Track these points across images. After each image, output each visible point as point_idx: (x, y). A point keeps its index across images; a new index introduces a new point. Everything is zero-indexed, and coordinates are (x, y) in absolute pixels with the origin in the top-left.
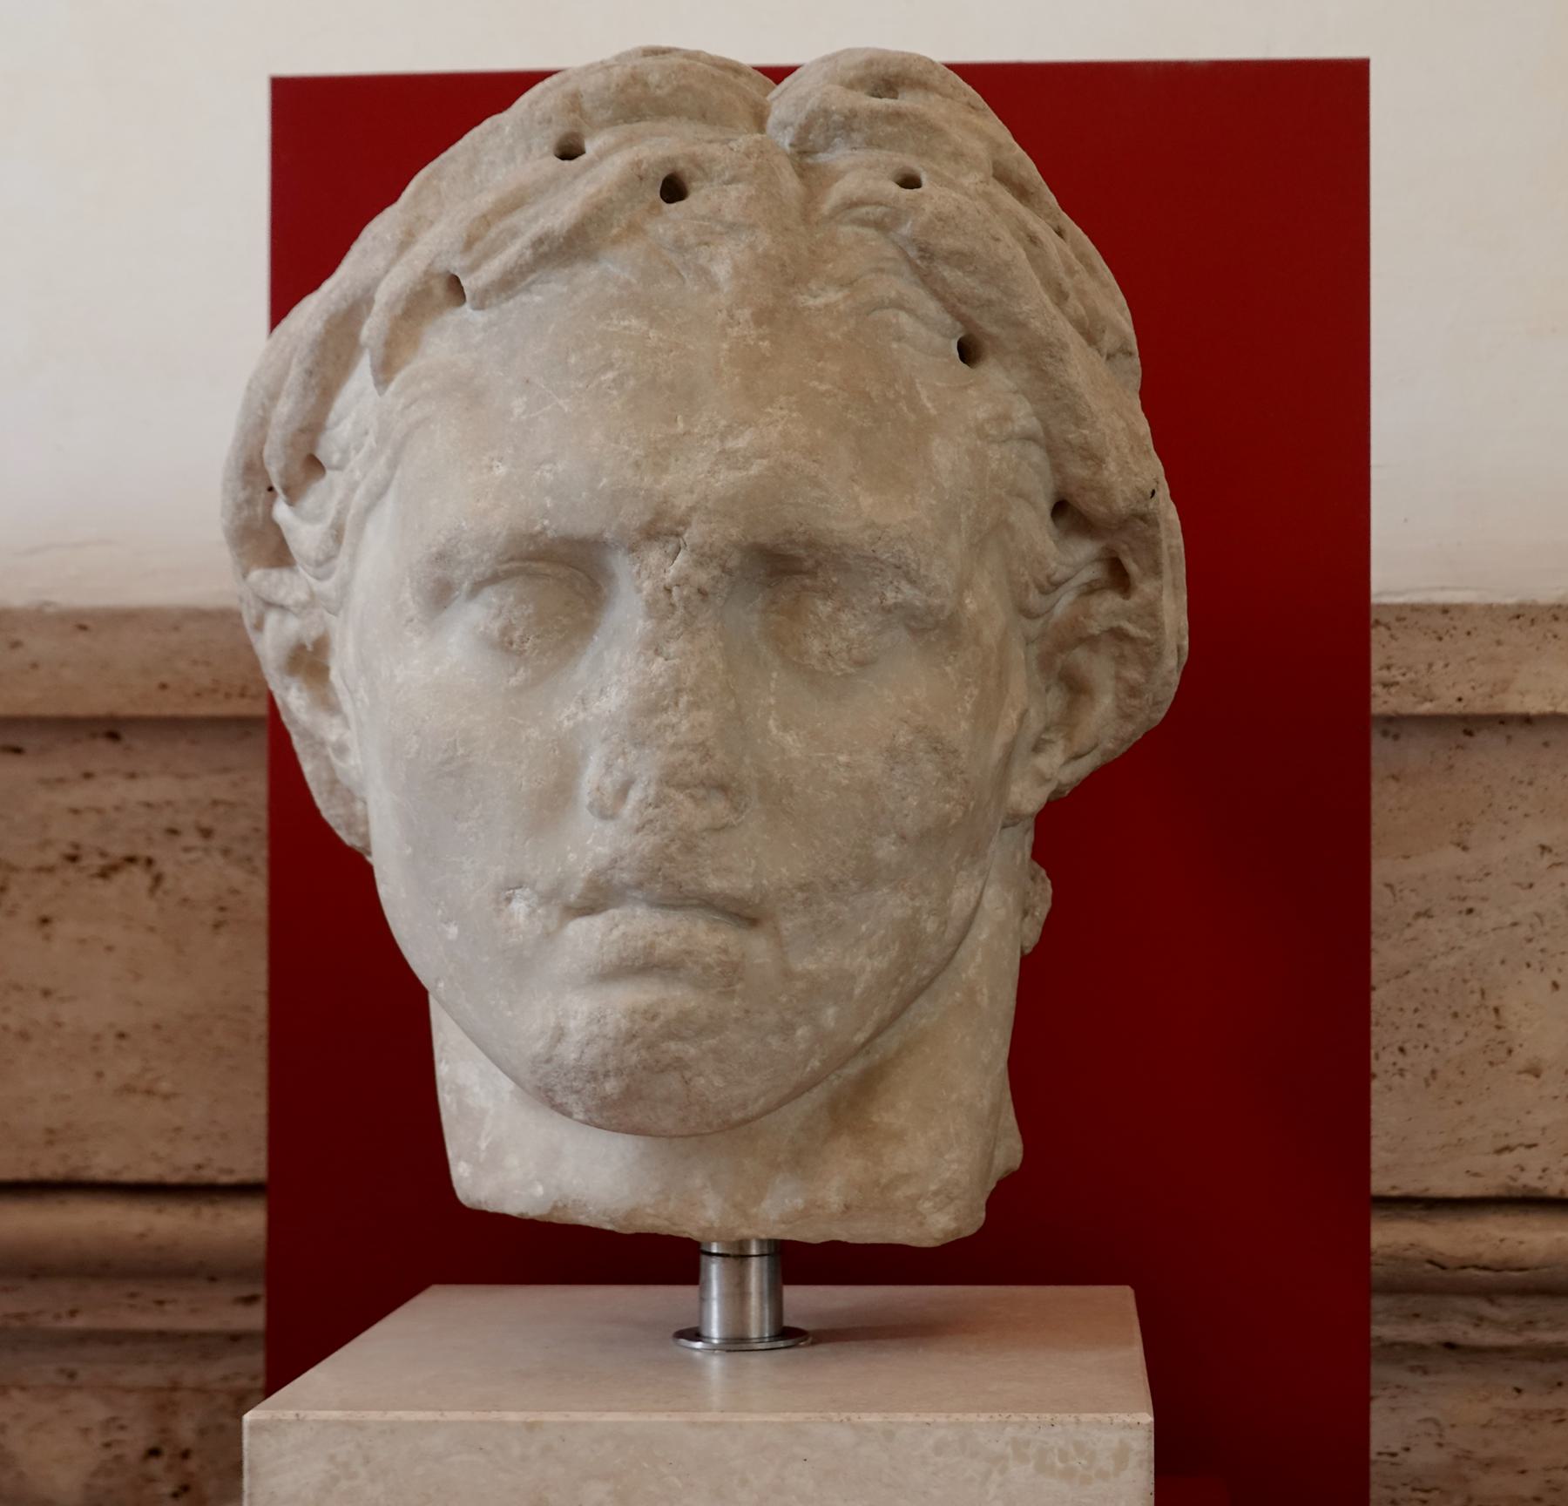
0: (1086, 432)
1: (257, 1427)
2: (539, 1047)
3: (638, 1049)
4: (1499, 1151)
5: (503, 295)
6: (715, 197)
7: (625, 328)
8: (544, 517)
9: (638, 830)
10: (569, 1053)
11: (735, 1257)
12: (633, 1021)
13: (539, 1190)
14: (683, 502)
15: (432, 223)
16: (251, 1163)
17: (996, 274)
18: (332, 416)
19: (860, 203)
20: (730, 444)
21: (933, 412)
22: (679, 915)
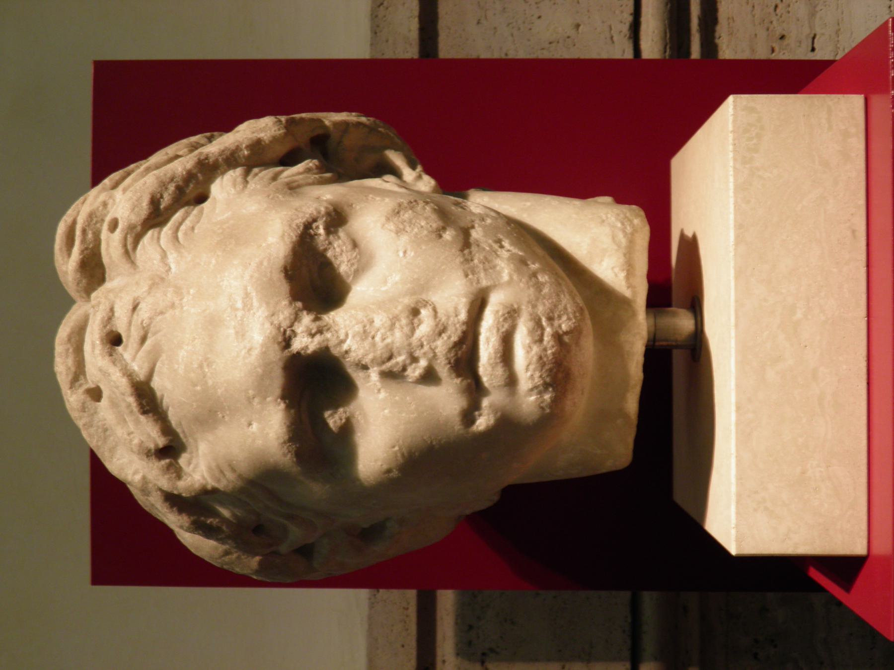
0: (244, 146)
4: (613, 42)
5: (213, 465)
16: (624, 596)
17: (164, 185)
21: (230, 213)
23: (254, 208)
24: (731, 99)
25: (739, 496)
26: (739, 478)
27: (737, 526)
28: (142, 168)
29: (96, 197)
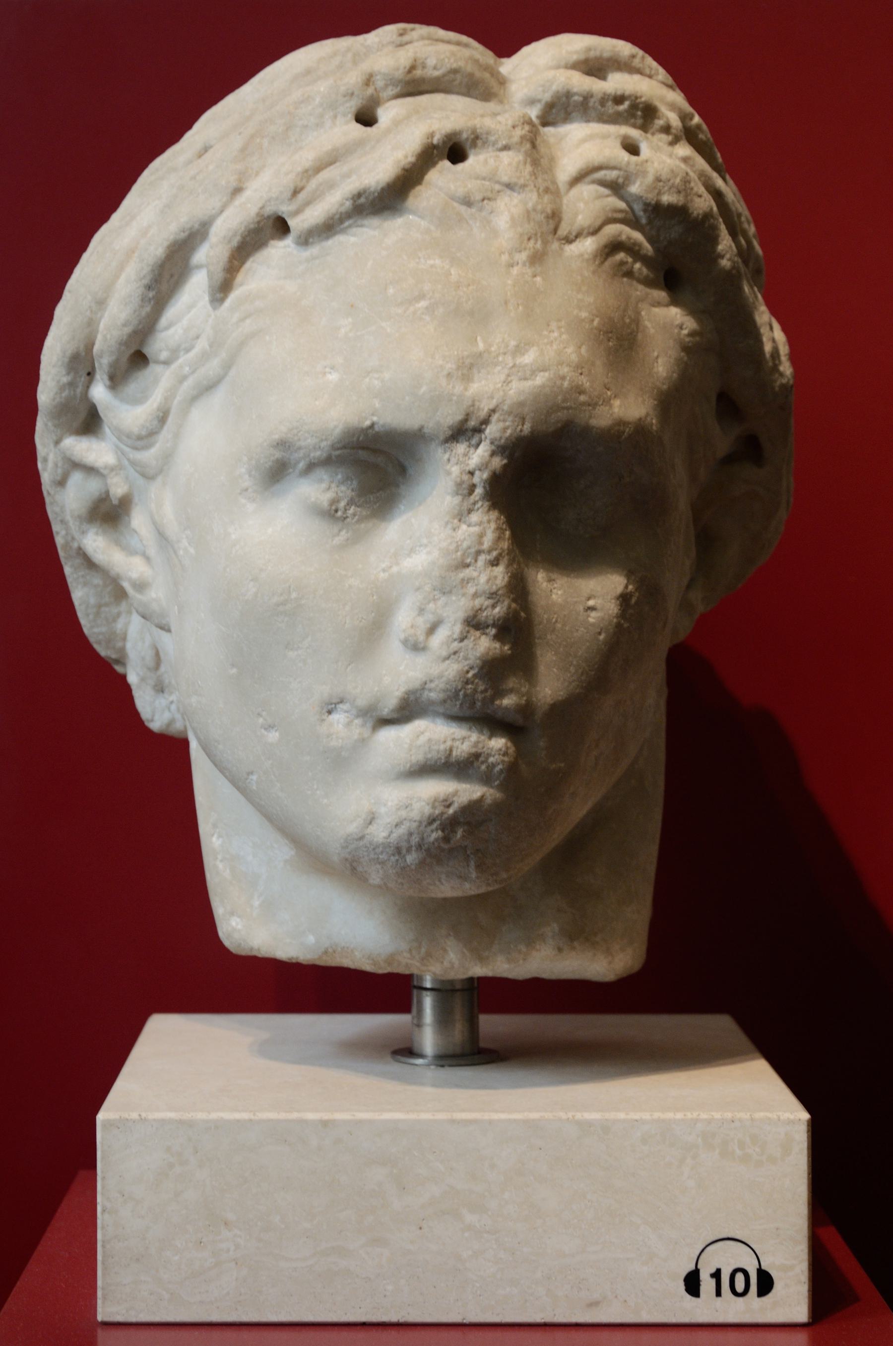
1: (109, 1124)
2: (352, 828)
3: (437, 829)
6: (491, 161)
7: (432, 266)
8: (373, 415)
9: (448, 658)
10: (379, 833)
11: (447, 991)
12: (434, 807)
13: (311, 939)
14: (485, 407)
15: (257, 174)
18: (163, 321)
19: (599, 168)
20: (520, 360)
22: (465, 726)
23: (661, 369)
24: (805, 1116)
25: (190, 1124)
26: (218, 1125)
27: (143, 1120)
28: (719, 183)
29: (673, 107)
